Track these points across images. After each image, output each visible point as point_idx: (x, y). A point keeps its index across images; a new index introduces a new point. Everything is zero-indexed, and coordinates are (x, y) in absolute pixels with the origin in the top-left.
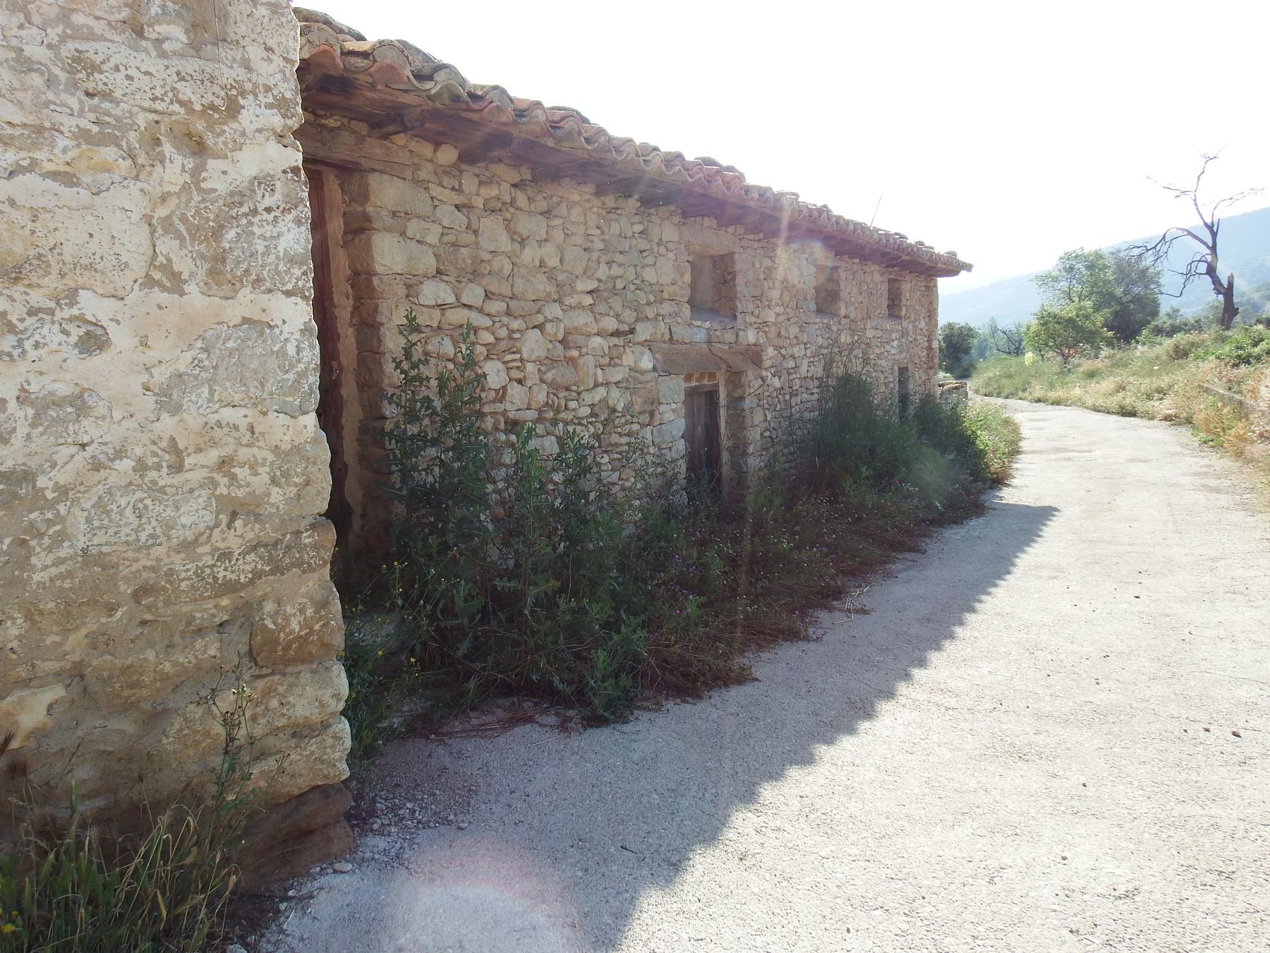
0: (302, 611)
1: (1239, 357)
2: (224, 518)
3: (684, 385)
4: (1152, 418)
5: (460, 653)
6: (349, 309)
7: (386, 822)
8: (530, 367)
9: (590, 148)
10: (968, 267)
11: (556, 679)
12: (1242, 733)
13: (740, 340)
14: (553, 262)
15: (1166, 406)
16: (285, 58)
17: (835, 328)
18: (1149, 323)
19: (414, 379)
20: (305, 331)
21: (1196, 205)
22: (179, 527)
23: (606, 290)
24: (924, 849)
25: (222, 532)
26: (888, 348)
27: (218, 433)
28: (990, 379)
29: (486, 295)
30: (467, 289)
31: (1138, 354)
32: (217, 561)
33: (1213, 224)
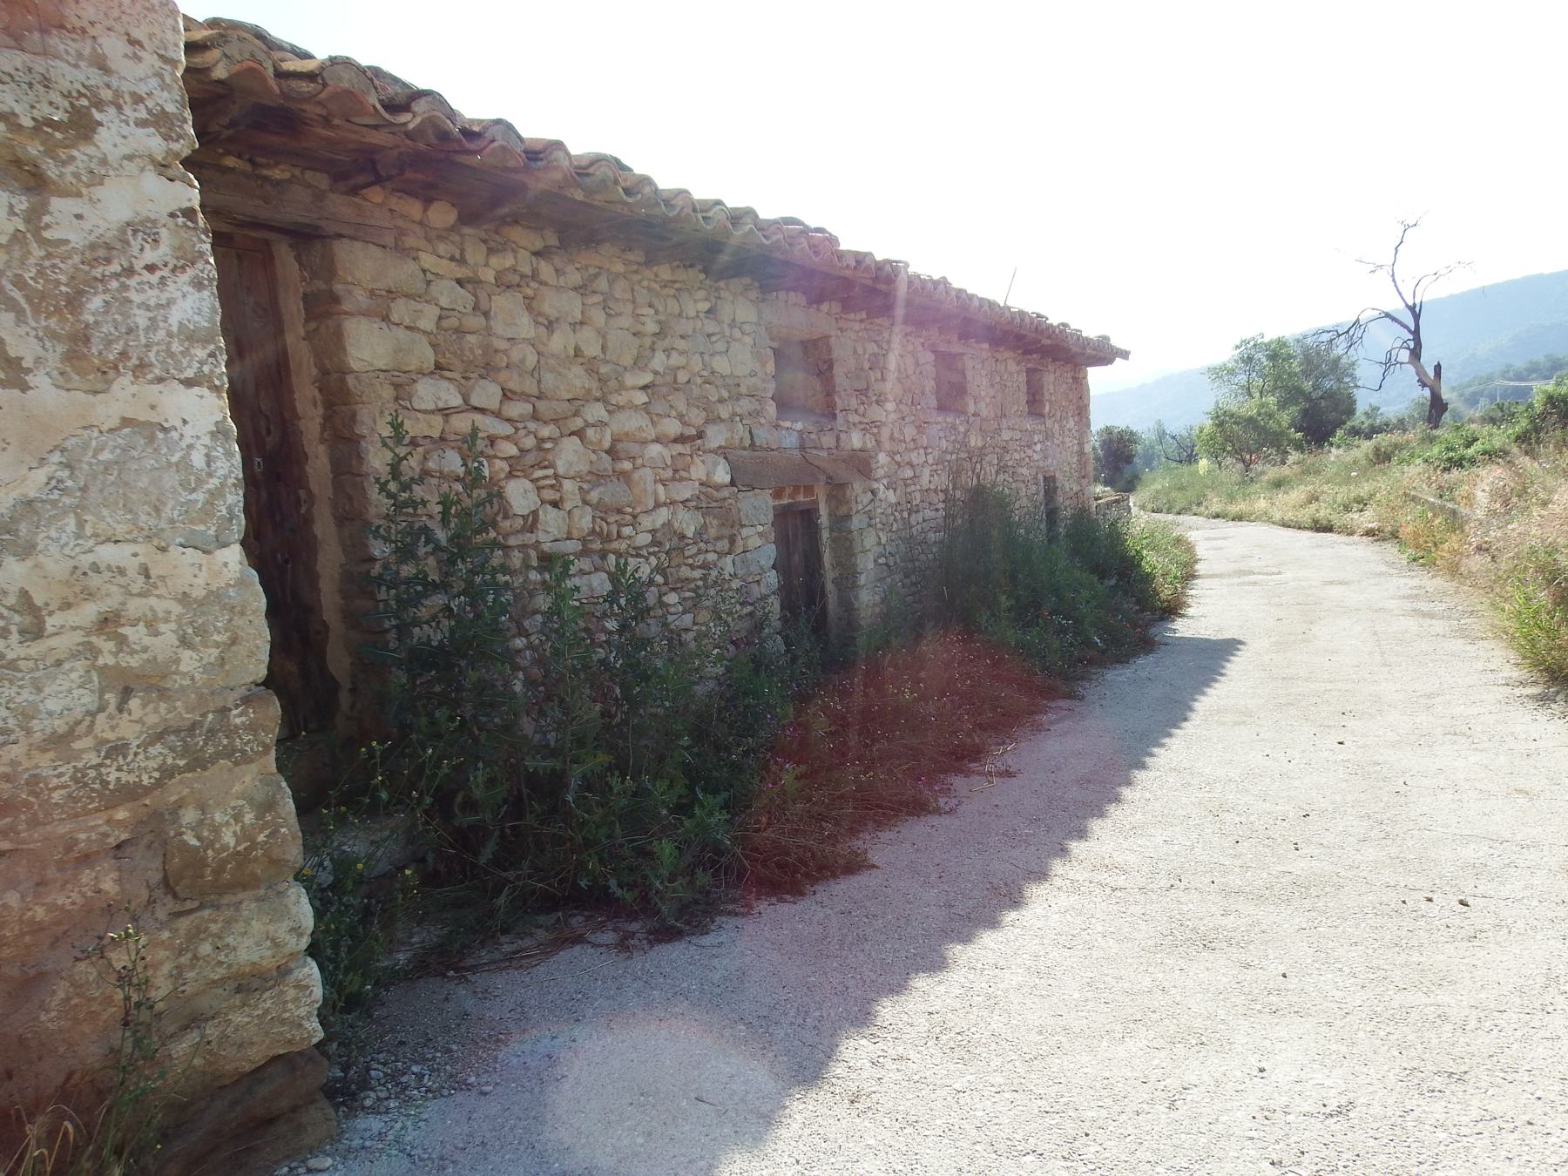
0: (237, 817)
1: (1450, 460)
2: (112, 698)
3: (771, 502)
4: (1352, 533)
5: (483, 860)
6: (318, 420)
7: (383, 1095)
8: (568, 485)
9: (630, 200)
10: (1125, 355)
11: (613, 883)
12: (1470, 901)
13: (842, 444)
14: (592, 350)
15: (1368, 519)
16: (161, 57)
17: (962, 429)
18: (1344, 423)
19: (405, 504)
20: (219, 432)
21: (1394, 280)
22: (43, 716)
23: (664, 385)
24: (1086, 1070)
25: (111, 717)
26: (1030, 452)
27: (95, 581)
28: (1157, 492)
29: (504, 395)
30: (477, 387)
31: (1332, 459)
32: (105, 758)
33: (1415, 305)
